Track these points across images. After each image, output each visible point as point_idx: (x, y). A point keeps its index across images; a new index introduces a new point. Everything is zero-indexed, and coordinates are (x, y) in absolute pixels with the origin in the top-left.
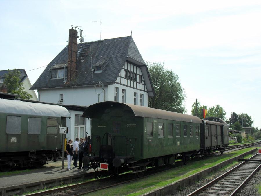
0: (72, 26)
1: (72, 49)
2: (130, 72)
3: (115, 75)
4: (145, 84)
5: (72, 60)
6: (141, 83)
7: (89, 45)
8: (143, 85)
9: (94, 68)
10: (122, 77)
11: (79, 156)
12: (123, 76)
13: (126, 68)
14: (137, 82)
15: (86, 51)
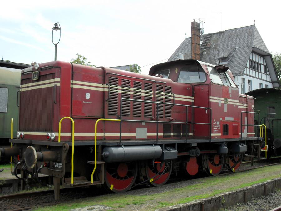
0: (194, 18)
1: (196, 41)
2: (254, 63)
3: (242, 66)
4: (269, 75)
5: (196, 53)
6: (266, 74)
7: (210, 37)
8: (267, 76)
9: (219, 59)
10: (248, 68)
11: (127, 176)
12: (248, 66)
13: (251, 58)
14: (261, 73)
15: (208, 43)
